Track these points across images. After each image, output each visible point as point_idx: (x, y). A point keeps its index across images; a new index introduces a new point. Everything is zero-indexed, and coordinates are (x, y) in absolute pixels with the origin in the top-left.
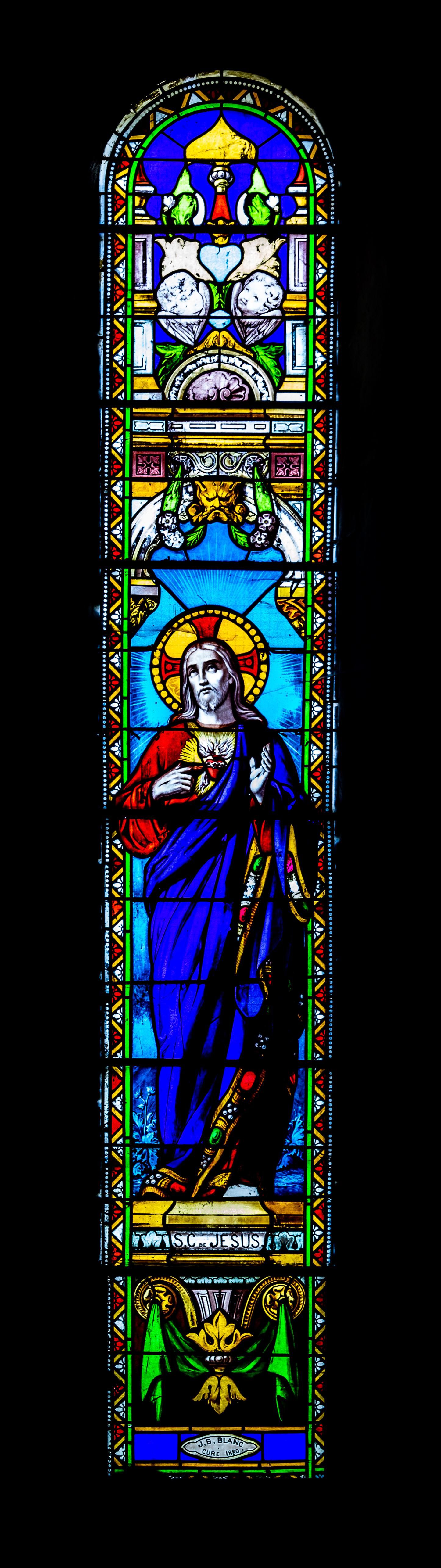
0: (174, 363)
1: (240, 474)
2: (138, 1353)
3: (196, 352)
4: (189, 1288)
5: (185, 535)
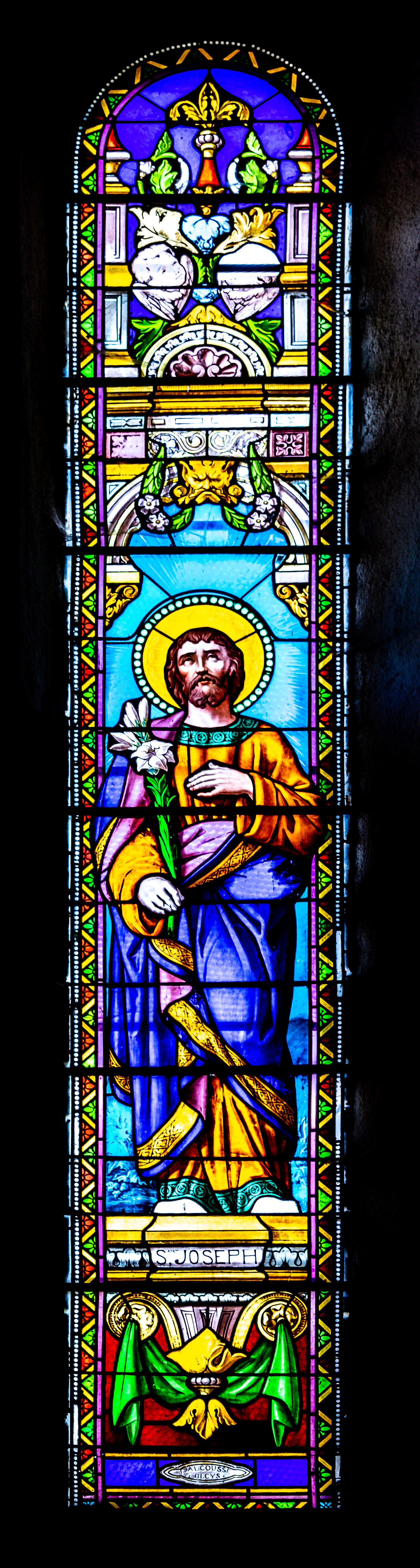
0: (150, 338)
3: (178, 327)
4: (171, 1305)
5: (171, 518)
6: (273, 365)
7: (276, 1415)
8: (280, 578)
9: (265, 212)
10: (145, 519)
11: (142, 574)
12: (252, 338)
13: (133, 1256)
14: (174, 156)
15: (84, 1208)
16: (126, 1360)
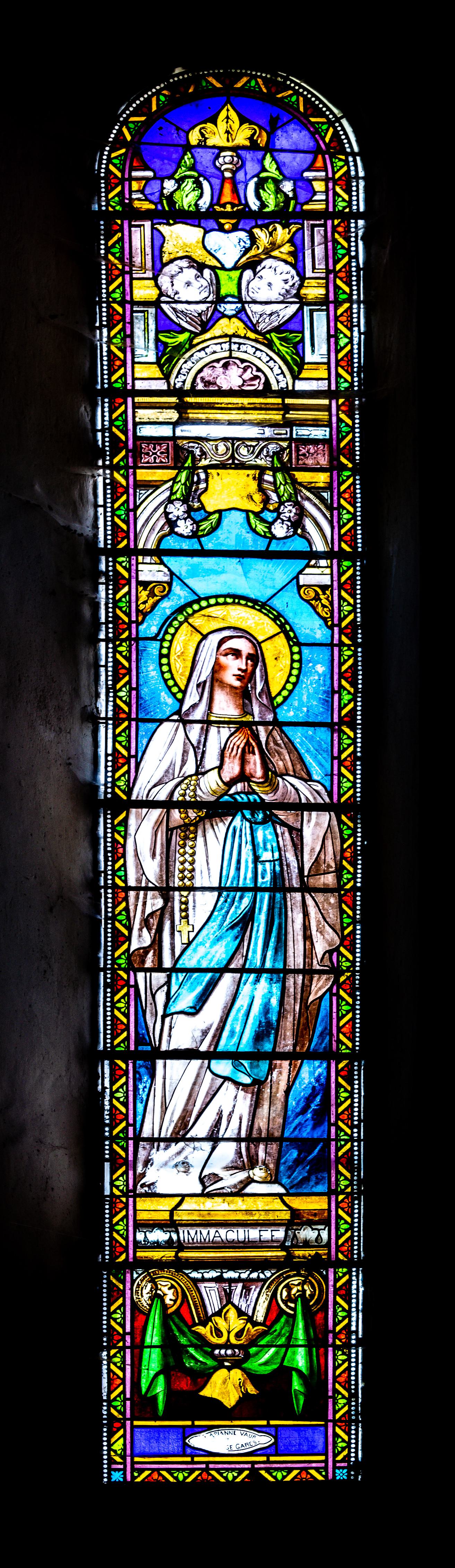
1: (259, 462)
2: (138, 1347)
6: (296, 377)
7: (296, 1384)
8: (303, 580)
9: (284, 228)
10: (172, 524)
11: (172, 574)
12: (274, 351)
13: (158, 1236)
14: (196, 174)
15: (115, 1191)
16: (153, 1335)
